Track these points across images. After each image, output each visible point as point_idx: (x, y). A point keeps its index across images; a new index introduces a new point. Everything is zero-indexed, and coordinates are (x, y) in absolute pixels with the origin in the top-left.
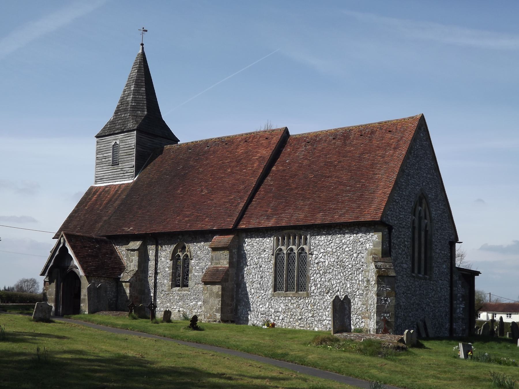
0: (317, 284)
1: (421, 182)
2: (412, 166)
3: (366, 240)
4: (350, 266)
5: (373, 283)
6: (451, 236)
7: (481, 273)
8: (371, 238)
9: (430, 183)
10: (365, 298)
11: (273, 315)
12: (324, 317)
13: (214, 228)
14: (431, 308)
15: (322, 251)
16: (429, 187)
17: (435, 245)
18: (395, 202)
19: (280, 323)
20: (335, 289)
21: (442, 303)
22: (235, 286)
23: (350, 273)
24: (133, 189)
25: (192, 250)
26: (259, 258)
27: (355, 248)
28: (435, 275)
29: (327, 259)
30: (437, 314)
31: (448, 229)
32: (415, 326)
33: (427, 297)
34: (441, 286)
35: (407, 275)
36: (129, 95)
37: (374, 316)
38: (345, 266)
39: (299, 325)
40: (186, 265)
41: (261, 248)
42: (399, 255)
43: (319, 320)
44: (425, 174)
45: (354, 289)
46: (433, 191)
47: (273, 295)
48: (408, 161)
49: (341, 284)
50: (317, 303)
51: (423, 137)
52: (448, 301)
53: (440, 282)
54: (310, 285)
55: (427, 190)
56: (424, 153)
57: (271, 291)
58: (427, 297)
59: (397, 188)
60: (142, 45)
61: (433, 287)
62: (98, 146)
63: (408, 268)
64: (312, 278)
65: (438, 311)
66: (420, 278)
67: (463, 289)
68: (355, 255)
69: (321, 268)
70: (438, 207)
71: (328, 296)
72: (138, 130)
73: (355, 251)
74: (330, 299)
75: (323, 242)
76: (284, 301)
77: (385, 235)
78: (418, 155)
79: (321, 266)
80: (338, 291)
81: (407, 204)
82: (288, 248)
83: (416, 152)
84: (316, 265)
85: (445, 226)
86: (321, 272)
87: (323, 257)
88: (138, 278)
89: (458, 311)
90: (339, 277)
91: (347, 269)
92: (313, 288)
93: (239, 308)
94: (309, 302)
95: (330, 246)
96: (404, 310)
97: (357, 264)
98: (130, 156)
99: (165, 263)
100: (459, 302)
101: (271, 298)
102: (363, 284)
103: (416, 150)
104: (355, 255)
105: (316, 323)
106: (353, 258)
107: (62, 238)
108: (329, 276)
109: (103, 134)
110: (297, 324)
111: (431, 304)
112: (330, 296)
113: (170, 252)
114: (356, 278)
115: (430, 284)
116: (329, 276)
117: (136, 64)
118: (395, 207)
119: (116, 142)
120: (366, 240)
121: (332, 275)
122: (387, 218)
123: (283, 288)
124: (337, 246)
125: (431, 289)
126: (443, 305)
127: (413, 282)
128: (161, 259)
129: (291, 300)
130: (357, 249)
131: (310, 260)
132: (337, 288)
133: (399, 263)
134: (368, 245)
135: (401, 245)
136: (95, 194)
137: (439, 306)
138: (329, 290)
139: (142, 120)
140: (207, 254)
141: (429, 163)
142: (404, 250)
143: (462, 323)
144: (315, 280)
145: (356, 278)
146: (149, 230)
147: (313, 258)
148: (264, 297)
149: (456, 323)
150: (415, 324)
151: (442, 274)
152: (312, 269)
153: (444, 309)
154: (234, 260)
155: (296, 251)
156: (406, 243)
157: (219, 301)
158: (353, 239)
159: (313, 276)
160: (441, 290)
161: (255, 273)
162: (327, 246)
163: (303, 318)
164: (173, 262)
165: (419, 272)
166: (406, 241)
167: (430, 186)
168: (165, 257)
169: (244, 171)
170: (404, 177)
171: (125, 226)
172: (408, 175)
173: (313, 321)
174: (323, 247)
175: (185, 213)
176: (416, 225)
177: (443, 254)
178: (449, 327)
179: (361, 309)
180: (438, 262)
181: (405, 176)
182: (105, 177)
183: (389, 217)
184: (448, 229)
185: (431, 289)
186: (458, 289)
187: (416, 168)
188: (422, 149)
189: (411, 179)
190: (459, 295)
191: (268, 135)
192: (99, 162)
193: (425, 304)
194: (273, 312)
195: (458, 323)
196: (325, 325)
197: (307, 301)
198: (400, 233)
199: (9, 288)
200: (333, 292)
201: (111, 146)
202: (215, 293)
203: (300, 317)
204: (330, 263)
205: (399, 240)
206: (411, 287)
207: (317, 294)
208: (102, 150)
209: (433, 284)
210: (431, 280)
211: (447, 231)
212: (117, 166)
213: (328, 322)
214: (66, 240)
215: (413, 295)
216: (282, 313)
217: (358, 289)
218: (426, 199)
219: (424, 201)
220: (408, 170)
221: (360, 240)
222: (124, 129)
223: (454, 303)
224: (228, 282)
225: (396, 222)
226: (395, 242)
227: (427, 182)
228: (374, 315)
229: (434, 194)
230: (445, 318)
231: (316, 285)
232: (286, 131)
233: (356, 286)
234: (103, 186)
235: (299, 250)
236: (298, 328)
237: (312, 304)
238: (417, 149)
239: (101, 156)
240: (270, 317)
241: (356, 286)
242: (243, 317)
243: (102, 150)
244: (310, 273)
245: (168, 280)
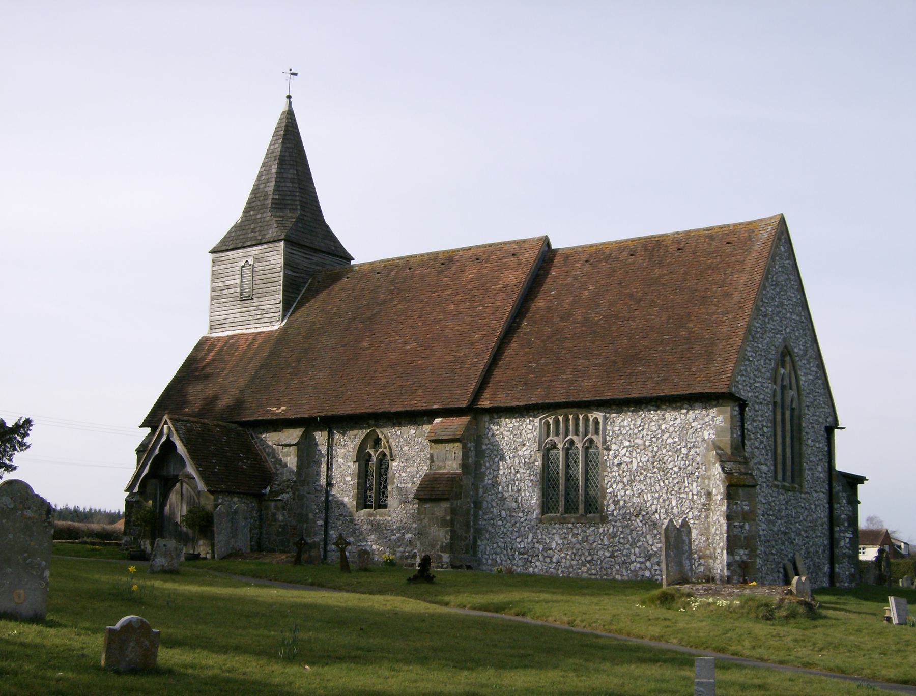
0: (619, 501)
1: (784, 328)
3: (704, 424)
4: (676, 469)
5: (719, 497)
6: (828, 417)
7: (867, 480)
8: (711, 422)
9: (796, 329)
10: (704, 524)
11: (540, 555)
12: (633, 557)
13: (435, 407)
15: (625, 445)
16: (796, 336)
17: (806, 433)
18: (748, 360)
19: (554, 568)
20: (650, 509)
22: (472, 506)
23: (675, 481)
24: (280, 340)
25: (394, 444)
27: (685, 438)
28: (808, 484)
29: (636, 458)
30: (811, 550)
31: (823, 405)
32: (781, 570)
33: (796, 521)
34: (817, 502)
36: (268, 181)
37: (722, 555)
38: (667, 470)
39: (587, 572)
40: (383, 471)
41: (518, 440)
42: (756, 450)
43: (624, 562)
45: (683, 509)
46: (801, 343)
47: (541, 521)
48: (764, 292)
49: (661, 500)
50: (619, 533)
51: (784, 252)
52: (827, 527)
53: (815, 494)
54: (605, 502)
55: (792, 341)
56: (787, 279)
58: (796, 521)
59: (750, 337)
60: (289, 97)
61: (804, 504)
62: (215, 268)
63: (769, 471)
64: (609, 491)
65: (813, 544)
66: (788, 490)
67: (849, 506)
68: (684, 451)
69: (625, 474)
70: (809, 369)
71: (637, 520)
72: (288, 241)
74: (642, 527)
75: (628, 429)
76: (559, 531)
77: (735, 415)
78: (779, 282)
79: (625, 469)
80: (656, 511)
82: (566, 439)
83: (774, 277)
84: (616, 469)
85: (819, 400)
86: (625, 480)
87: (628, 454)
88: (297, 493)
89: (842, 543)
91: (671, 474)
92: (612, 507)
93: (479, 543)
94: (606, 532)
95: (641, 436)
96: (765, 543)
97: (688, 466)
98: (274, 284)
100: (843, 528)
101: (537, 525)
102: (700, 499)
103: (774, 273)
104: (684, 451)
105: (618, 567)
106: (682, 456)
107: (165, 427)
108: (639, 487)
109: (224, 248)
110: (584, 569)
111: (803, 532)
112: (641, 521)
113: (353, 448)
114: (687, 490)
115: (801, 498)
117: (280, 129)
118: (748, 369)
119: (247, 261)
120: (704, 424)
121: (645, 485)
122: (738, 387)
123: (557, 509)
124: (652, 436)
125: (802, 508)
126: (819, 534)
127: (776, 495)
128: (337, 461)
129: (572, 529)
130: (688, 440)
131: (606, 460)
132: (654, 507)
133: (756, 464)
135: (758, 433)
136: (210, 351)
137: (814, 536)
138: (641, 510)
139: (293, 223)
140: (421, 451)
141: (793, 295)
143: (849, 563)
144: (615, 494)
145: (687, 490)
146: (315, 411)
147: (610, 457)
148: (524, 524)
149: (839, 564)
150: (780, 567)
151: (817, 481)
152: (610, 475)
153: (821, 541)
154: (470, 460)
155: (579, 445)
156: (765, 429)
157: (447, 532)
158: (681, 423)
159: (611, 486)
160: (816, 508)
161: (507, 483)
162: (634, 436)
163: (595, 559)
164: (359, 465)
165: (784, 480)
166: (765, 427)
167: (797, 334)
168: (345, 457)
169: (478, 309)
170: (760, 319)
171: (274, 406)
172: (765, 316)
173: (613, 563)
174: (627, 438)
175: (378, 381)
176: (778, 399)
177: (817, 447)
178: (829, 570)
180: (811, 462)
181: (761, 317)
182: (228, 321)
183: (740, 386)
184: (823, 405)
186: (841, 506)
188: (783, 272)
189: (769, 323)
190: (843, 516)
191: (512, 250)
192: (217, 296)
193: (793, 532)
194: (541, 549)
195: (841, 563)
196: (635, 571)
197: (601, 530)
198: (756, 413)
199: (91, 510)
200: (647, 514)
201: (239, 268)
202: (439, 518)
203: (589, 558)
204: (641, 464)
205: (755, 424)
206: (773, 504)
207: (618, 518)
208: (222, 275)
209: (804, 499)
211: (821, 410)
212: (250, 301)
213: (638, 565)
214: (173, 429)
215: (777, 518)
216: (557, 552)
217: (692, 508)
219: (788, 359)
220: (765, 307)
221: (693, 424)
222: (261, 239)
223: (836, 529)
224: (460, 498)
225: (750, 395)
226: (749, 427)
227: (791, 328)
228: (722, 551)
229: (802, 348)
230: (823, 556)
232: (546, 242)
233: (687, 504)
234: (225, 337)
235: (565, 444)
236: (585, 575)
237: (610, 534)
238: (776, 273)
239: (221, 284)
240: (536, 558)
241: (687, 504)
242: (487, 559)
243: (222, 275)
244: (606, 482)
245: (351, 497)
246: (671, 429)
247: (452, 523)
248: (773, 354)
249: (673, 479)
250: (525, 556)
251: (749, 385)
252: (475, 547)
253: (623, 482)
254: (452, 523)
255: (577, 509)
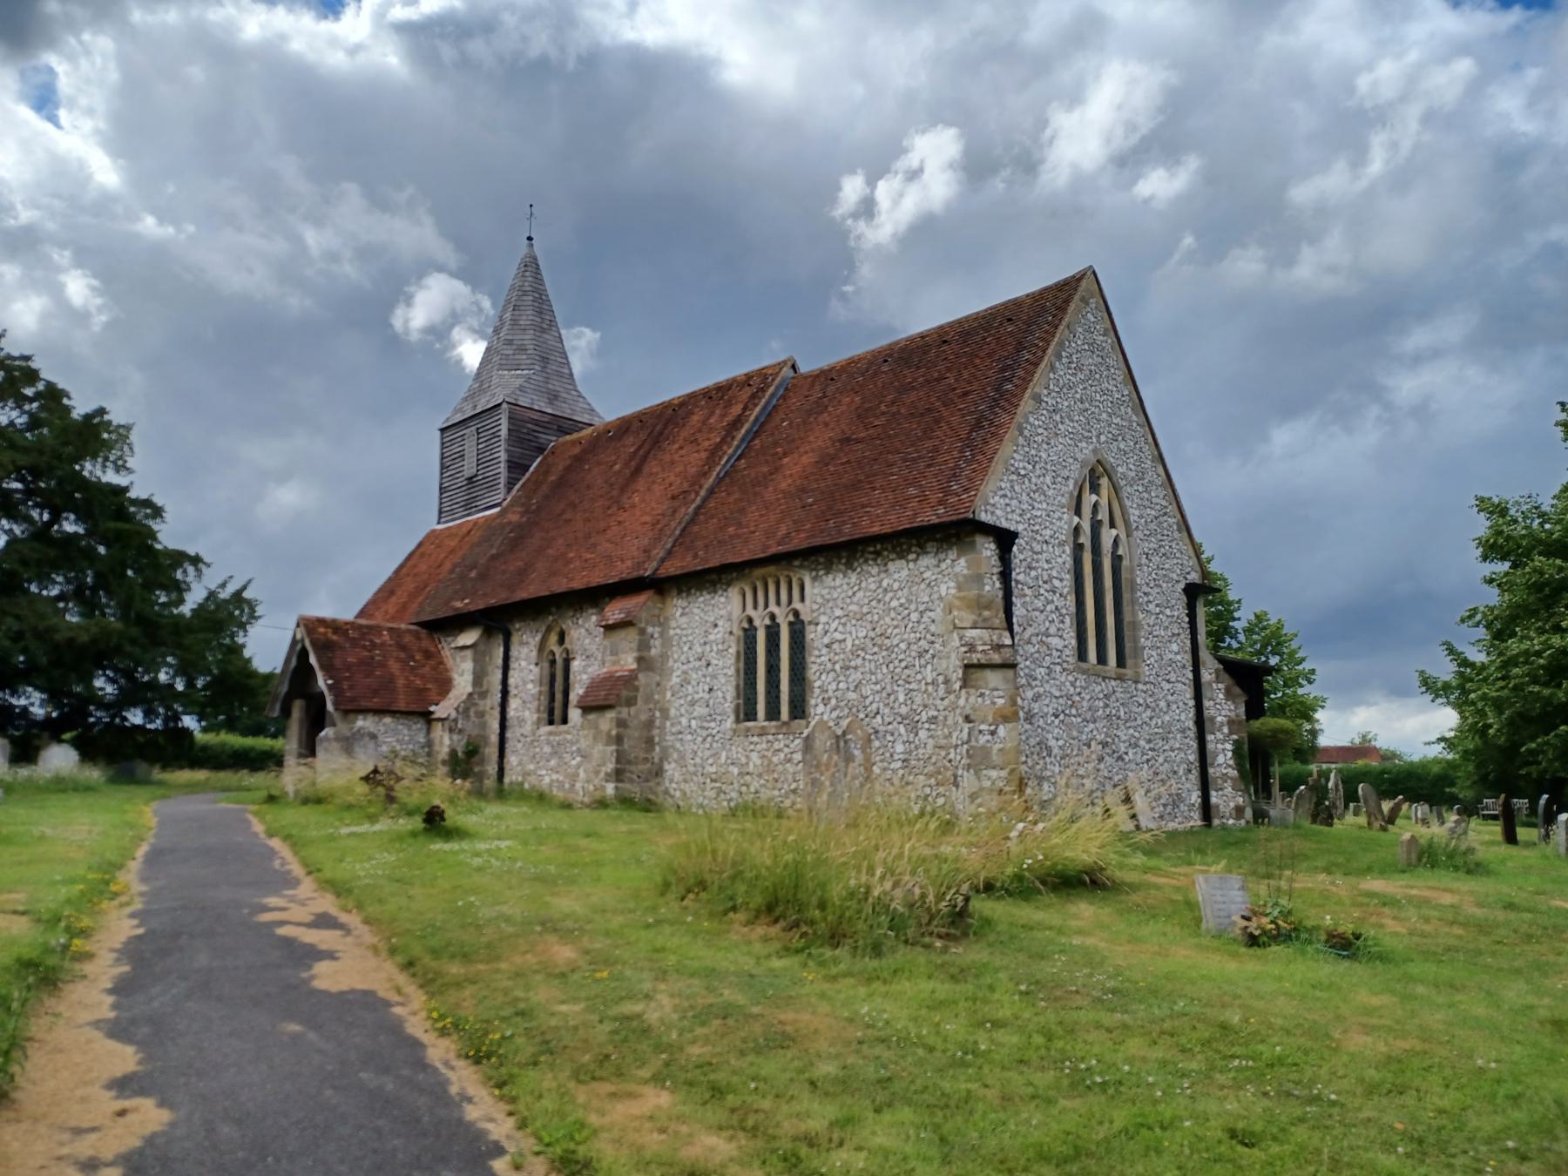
0: (829, 699)
2: (1065, 390)
4: (903, 646)
14: (1143, 754)
21: (1175, 739)
23: (903, 664)
26: (705, 643)
29: (850, 633)
31: (1178, 555)
34: (1170, 697)
35: (1065, 665)
42: (1037, 613)
44: (1104, 415)
53: (1166, 686)
57: (729, 723)
65: (1165, 761)
68: (914, 617)
73: (913, 607)
80: (878, 713)
81: (1054, 483)
84: (824, 651)
86: (837, 667)
89: (1221, 759)
90: (880, 676)
92: (821, 708)
99: (526, 671)
104: (914, 617)
108: (855, 676)
111: (1142, 743)
116: (855, 676)
125: (1140, 705)
132: (874, 706)
134: (943, 590)
137: (1166, 747)
142: (1053, 601)
156: (1056, 583)
165: (1102, 659)
176: (1085, 539)
179: (933, 760)
183: (998, 512)
184: (1178, 555)
185: (1140, 705)
187: (1078, 396)
190: (1219, 719)
195: (1221, 789)
204: (857, 642)
205: (1033, 573)
210: (1136, 682)
215: (1084, 720)
218: (1110, 479)
219: (1104, 481)
221: (925, 576)
231: (826, 702)
246: (896, 586)
247: (619, 740)
248: (1075, 472)
249: (901, 661)
250: (718, 785)
251: (1018, 511)
252: (659, 772)
253: (834, 670)
254: (619, 740)
255: (779, 713)
